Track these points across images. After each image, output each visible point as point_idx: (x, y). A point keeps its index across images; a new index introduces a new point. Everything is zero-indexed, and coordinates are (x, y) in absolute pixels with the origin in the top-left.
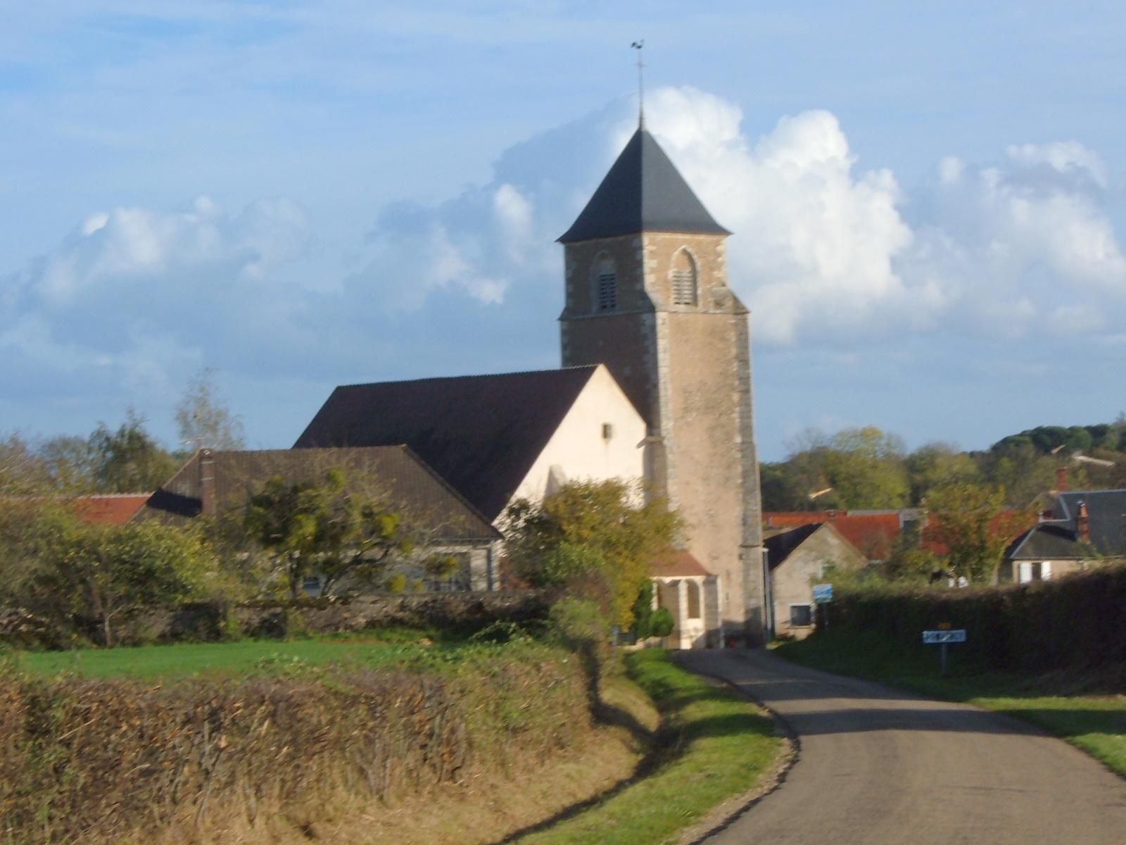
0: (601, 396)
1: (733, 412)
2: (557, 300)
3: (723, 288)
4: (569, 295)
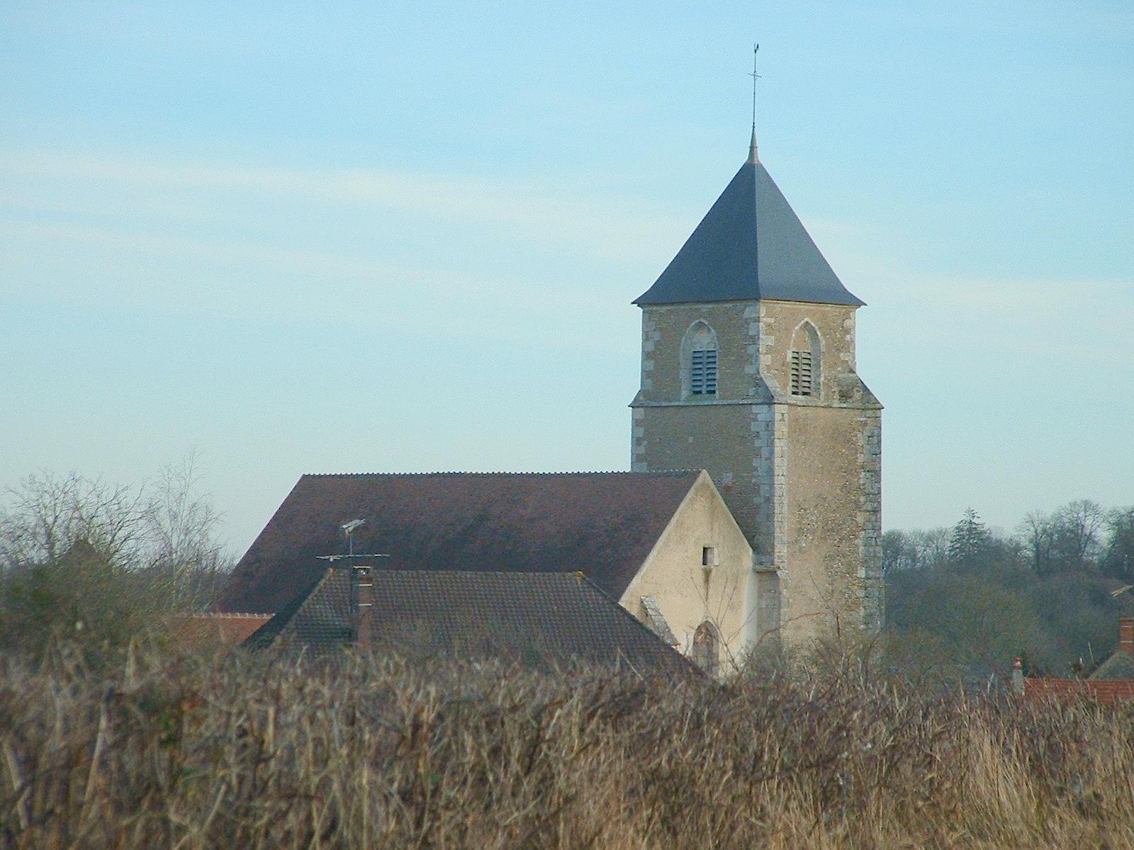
0: (696, 523)
1: (856, 537)
2: (632, 384)
3: (851, 375)
4: (646, 374)
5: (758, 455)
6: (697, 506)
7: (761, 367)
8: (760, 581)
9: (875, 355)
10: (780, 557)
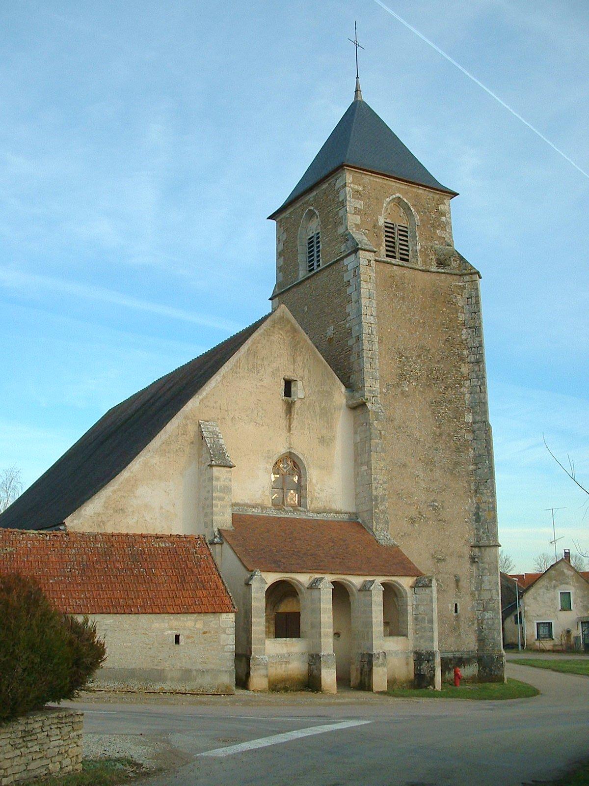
5: (350, 301)
6: (276, 337)
7: (349, 224)
8: (355, 417)
9: (472, 229)
10: (370, 392)
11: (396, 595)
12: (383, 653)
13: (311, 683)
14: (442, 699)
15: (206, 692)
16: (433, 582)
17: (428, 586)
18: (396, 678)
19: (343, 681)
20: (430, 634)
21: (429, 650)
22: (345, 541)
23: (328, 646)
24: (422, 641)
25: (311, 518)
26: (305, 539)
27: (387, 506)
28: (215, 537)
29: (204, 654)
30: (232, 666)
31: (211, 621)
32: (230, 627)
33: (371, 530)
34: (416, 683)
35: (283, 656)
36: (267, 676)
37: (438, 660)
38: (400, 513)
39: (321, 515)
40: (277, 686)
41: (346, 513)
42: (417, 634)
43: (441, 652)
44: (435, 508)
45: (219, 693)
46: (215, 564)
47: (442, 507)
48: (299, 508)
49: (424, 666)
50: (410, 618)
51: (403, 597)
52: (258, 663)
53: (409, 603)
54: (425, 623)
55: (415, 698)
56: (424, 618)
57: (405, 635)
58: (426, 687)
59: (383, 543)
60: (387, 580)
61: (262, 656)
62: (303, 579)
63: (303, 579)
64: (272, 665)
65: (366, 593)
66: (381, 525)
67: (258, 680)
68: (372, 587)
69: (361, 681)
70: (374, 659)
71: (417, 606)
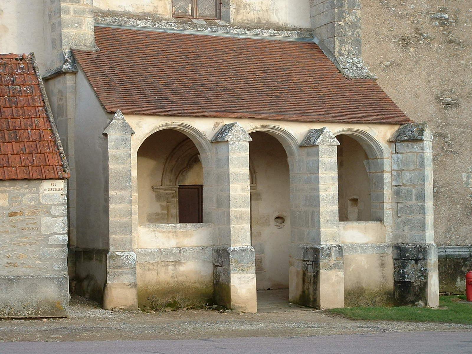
11: (367, 157)
12: (337, 248)
13: (216, 297)
14: (431, 325)
15: (16, 314)
16: (425, 133)
17: (418, 139)
18: (363, 288)
19: (272, 292)
20: (420, 217)
21: (419, 242)
22: (284, 71)
23: (241, 236)
24: (406, 228)
25: (236, 36)
26: (219, 67)
27: (359, 16)
28: (65, 61)
29: (12, 251)
30: (63, 270)
31: (24, 195)
32: (58, 205)
33: (333, 54)
34: (397, 295)
35: (169, 252)
36: (135, 285)
37: (433, 259)
38: (385, 31)
39: (252, 32)
40: (153, 302)
41: (293, 30)
42: (399, 217)
43: (439, 246)
44: (444, 23)
45: (39, 316)
46: (43, 100)
47: (456, 21)
48: (218, 22)
49: (410, 269)
50: (388, 192)
51: (376, 158)
52: (119, 264)
53: (387, 167)
54: (411, 200)
55: (384, 322)
56: (410, 192)
57: (380, 219)
58: (413, 303)
59: (350, 74)
60: (348, 130)
61: (126, 253)
62: (204, 127)
63: (204, 127)
64: (151, 267)
65: (311, 150)
66: (348, 47)
67: (120, 291)
68: (319, 141)
69: (303, 292)
70: (321, 257)
71: (400, 172)
